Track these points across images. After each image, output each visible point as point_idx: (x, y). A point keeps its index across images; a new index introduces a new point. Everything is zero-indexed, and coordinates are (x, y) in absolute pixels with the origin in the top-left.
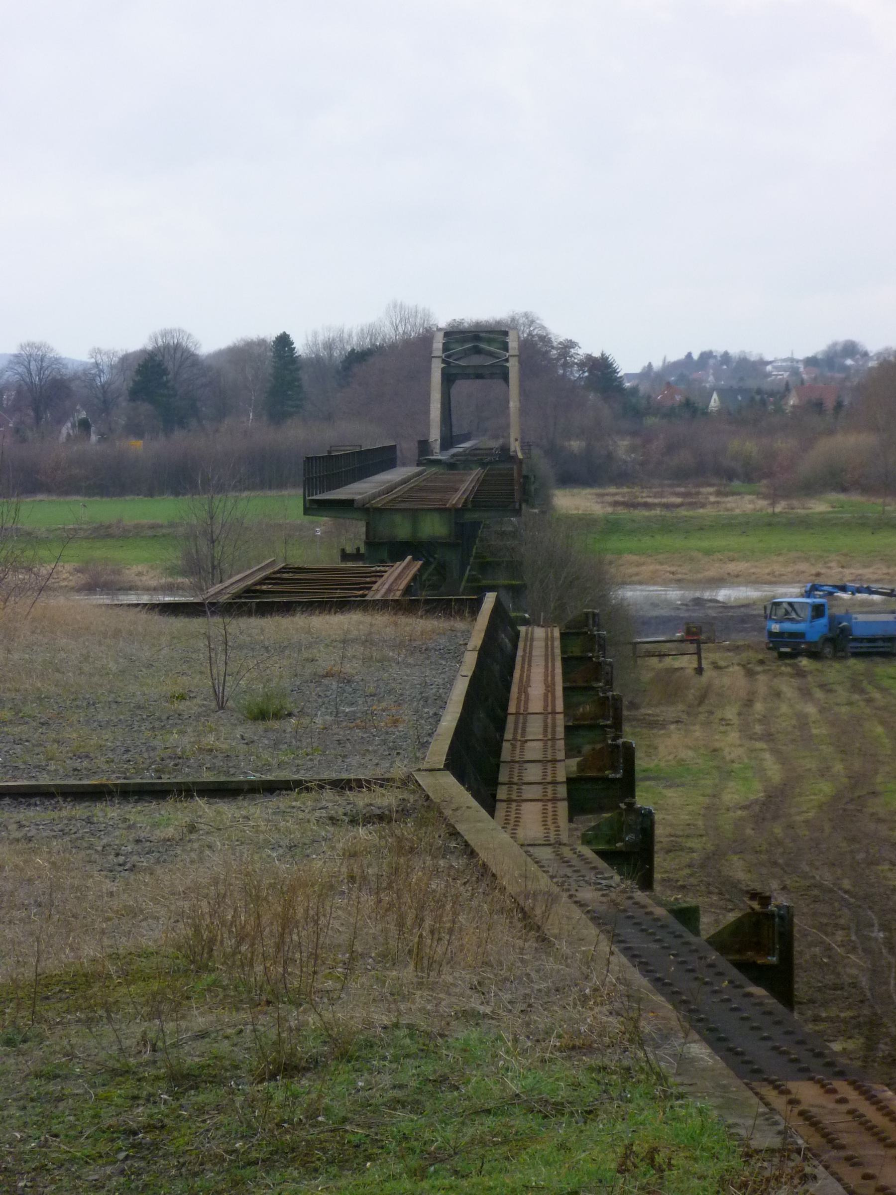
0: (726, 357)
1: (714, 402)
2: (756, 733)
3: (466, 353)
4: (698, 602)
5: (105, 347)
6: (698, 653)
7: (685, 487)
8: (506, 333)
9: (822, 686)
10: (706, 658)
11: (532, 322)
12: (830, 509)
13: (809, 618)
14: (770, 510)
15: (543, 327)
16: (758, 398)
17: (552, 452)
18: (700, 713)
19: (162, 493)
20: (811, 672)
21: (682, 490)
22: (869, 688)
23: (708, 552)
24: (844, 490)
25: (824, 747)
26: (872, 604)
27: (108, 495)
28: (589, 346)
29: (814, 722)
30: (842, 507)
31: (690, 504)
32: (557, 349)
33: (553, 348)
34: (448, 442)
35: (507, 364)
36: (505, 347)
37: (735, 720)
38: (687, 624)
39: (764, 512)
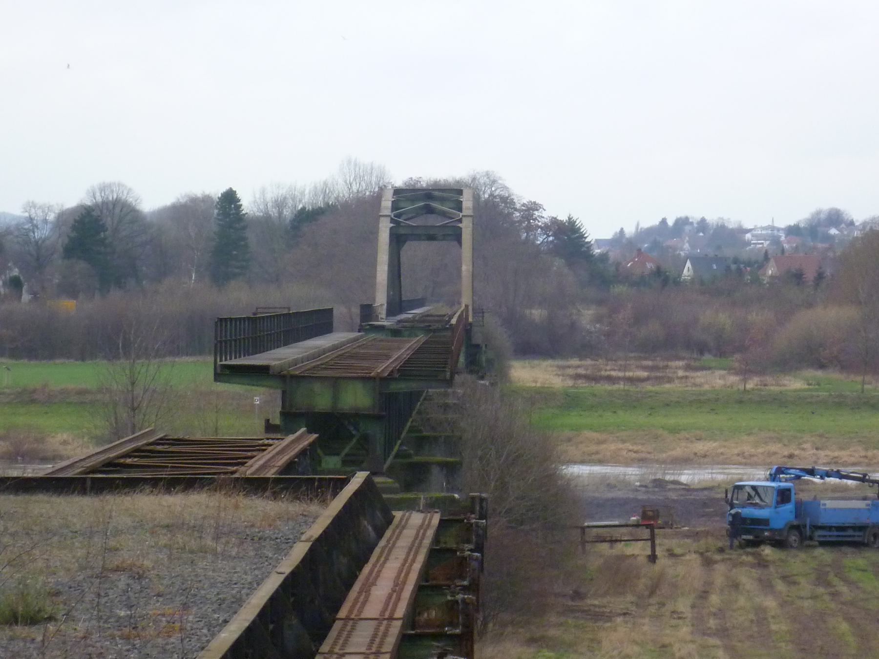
0: (703, 224)
1: (688, 272)
2: (709, 628)
3: (418, 213)
4: (659, 484)
5: (42, 199)
6: (652, 539)
7: (652, 360)
8: (460, 192)
9: (784, 578)
10: (660, 545)
11: (494, 182)
12: (807, 387)
13: (774, 502)
14: (741, 387)
15: (505, 188)
16: (733, 267)
17: (511, 321)
18: (649, 605)
19: (93, 356)
20: (774, 562)
21: (649, 363)
22: (836, 581)
23: (674, 430)
24: (822, 366)
25: (783, 644)
26: (846, 489)
27: (36, 357)
28: (555, 208)
29: (773, 617)
30: (819, 384)
31: (657, 378)
32: (519, 211)
33: (516, 210)
34: (396, 306)
35: (460, 225)
36: (459, 207)
37: (687, 612)
38: (644, 507)
39: (735, 388)
